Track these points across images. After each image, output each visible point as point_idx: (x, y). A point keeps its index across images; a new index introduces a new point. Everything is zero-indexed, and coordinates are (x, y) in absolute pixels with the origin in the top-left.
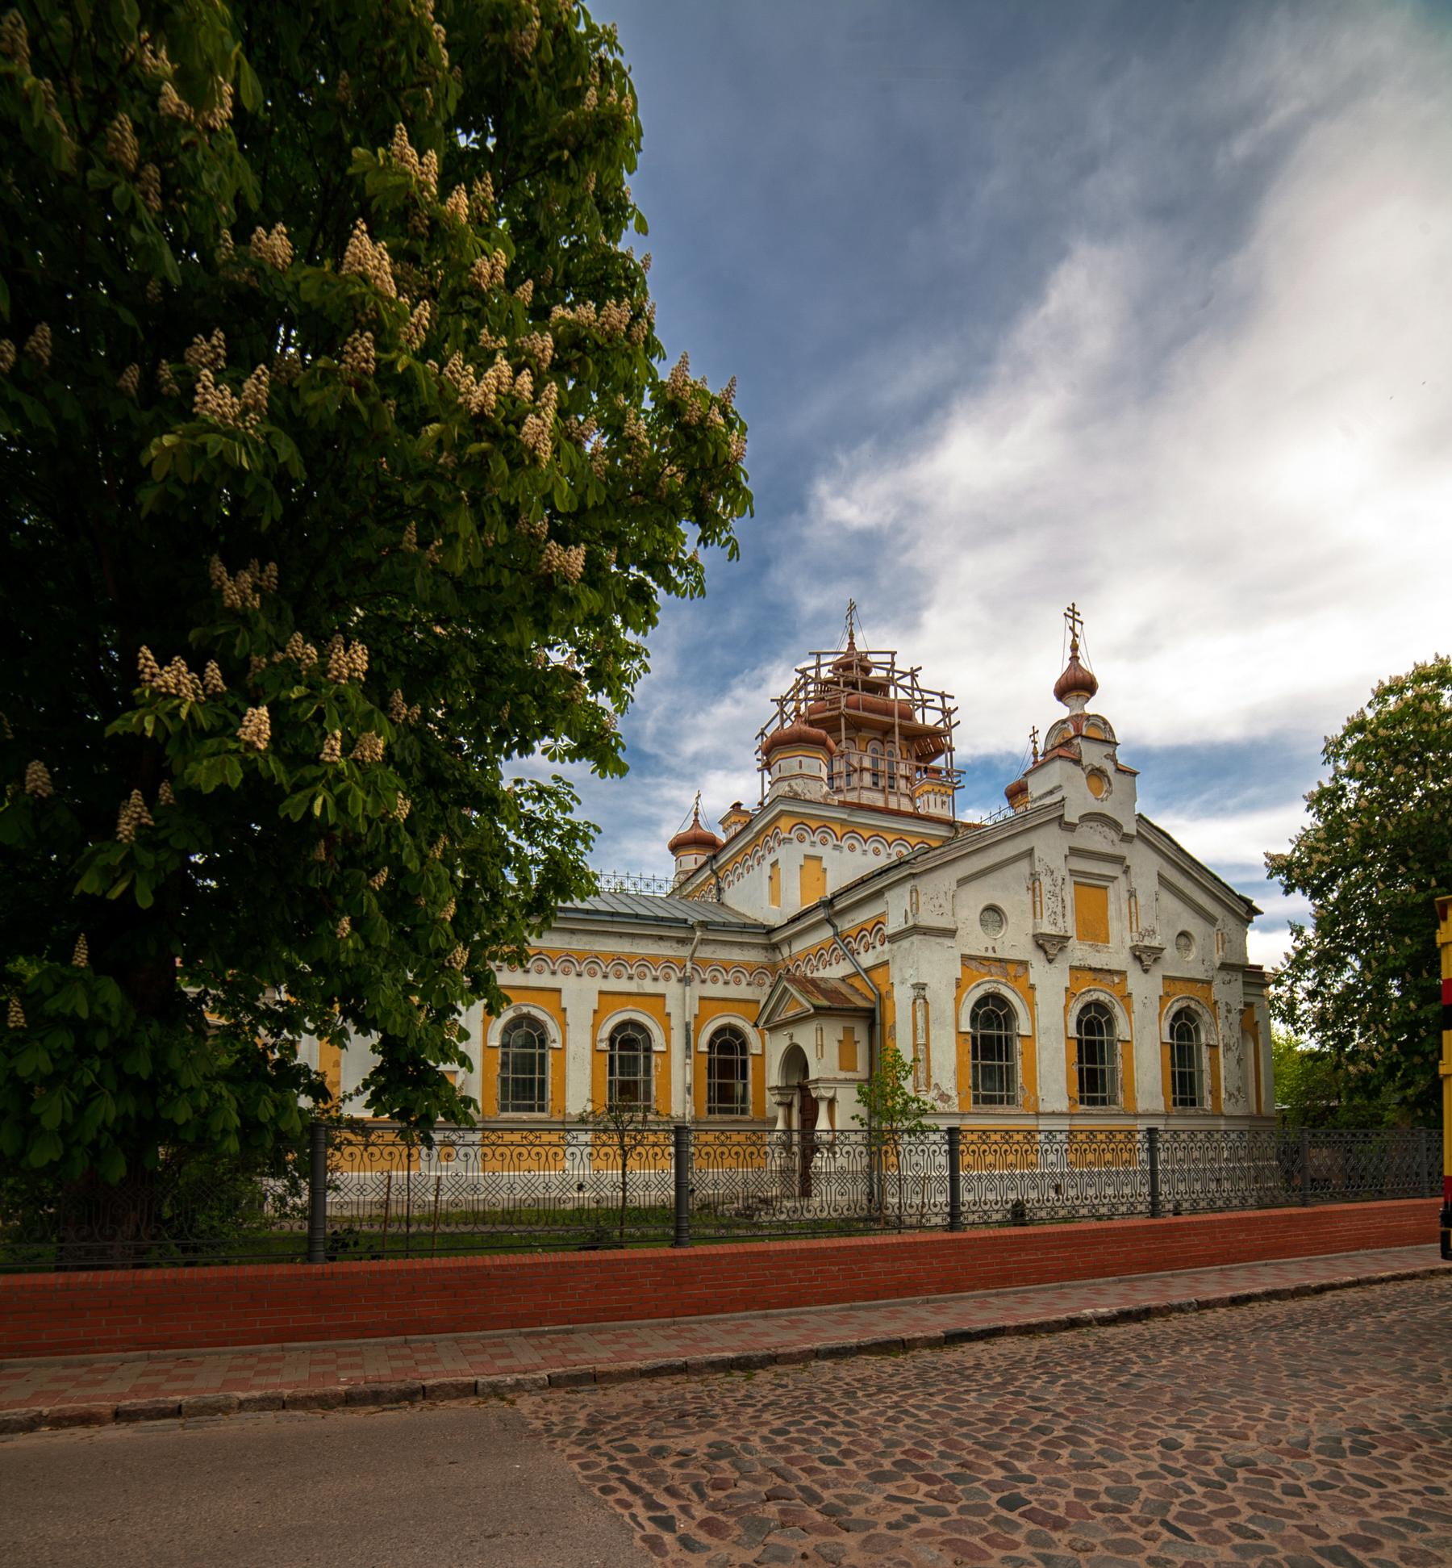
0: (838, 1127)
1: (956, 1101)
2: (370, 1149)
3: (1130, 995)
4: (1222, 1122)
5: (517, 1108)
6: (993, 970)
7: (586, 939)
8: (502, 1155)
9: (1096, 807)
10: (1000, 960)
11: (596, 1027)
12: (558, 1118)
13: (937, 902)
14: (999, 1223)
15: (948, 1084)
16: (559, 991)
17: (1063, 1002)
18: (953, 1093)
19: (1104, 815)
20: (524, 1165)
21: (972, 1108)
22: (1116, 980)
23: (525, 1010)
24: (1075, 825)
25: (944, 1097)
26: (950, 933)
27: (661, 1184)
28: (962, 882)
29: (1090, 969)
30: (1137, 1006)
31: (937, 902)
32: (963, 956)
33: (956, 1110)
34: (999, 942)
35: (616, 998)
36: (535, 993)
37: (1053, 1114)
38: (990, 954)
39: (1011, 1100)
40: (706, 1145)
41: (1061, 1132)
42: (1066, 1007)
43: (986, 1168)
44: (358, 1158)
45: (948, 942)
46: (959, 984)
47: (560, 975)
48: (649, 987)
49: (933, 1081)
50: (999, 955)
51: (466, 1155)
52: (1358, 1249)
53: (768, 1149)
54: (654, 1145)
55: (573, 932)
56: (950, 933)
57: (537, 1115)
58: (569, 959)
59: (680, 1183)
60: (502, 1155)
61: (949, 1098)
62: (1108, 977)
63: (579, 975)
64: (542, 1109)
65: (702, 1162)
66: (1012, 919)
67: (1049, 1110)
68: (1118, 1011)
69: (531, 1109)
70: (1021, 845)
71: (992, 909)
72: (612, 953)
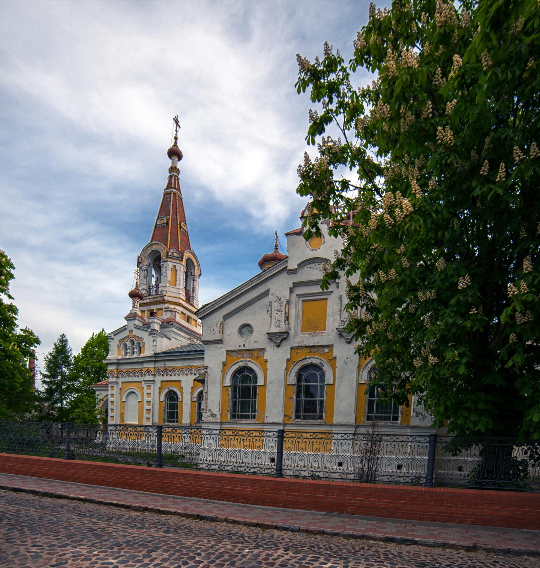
0: (353, 432)
1: (219, 417)
2: (356, 442)
3: (335, 358)
4: (409, 430)
5: (170, 421)
6: (245, 355)
7: (188, 361)
8: (320, 442)
9: (311, 254)
10: (249, 350)
11: (192, 393)
12: (180, 425)
13: (212, 329)
14: (269, 475)
15: (216, 410)
16: (180, 381)
17: (284, 366)
18: (218, 413)
19: (317, 258)
20: (197, 441)
21: (293, 420)
22: (326, 350)
23: (171, 388)
24: (296, 269)
25: (213, 415)
26: (220, 341)
27: (153, 445)
28: (226, 317)
29: (306, 347)
30: (338, 364)
31: (212, 329)
32: (227, 351)
33: (219, 421)
34: (247, 341)
35: (126, 384)
36: (174, 383)
37: (273, 424)
38: (242, 348)
39: (254, 417)
40: (256, 436)
41: (216, 430)
42: (287, 369)
43: (231, 446)
44: (397, 447)
45: (219, 346)
46: (224, 364)
47: (181, 375)
48: (174, 378)
49: (208, 408)
50: (246, 348)
51: (349, 444)
52: (191, 496)
53: (151, 433)
54: (140, 431)
55: (184, 360)
56: (220, 341)
57: (175, 424)
58: (181, 369)
59: (159, 447)
60: (320, 442)
61: (216, 415)
62: (321, 350)
63: (187, 375)
64: (177, 422)
65: (166, 439)
66: (255, 329)
67: (271, 421)
68: (327, 368)
69: (174, 422)
70: (261, 290)
71: (247, 326)
72: (197, 366)
